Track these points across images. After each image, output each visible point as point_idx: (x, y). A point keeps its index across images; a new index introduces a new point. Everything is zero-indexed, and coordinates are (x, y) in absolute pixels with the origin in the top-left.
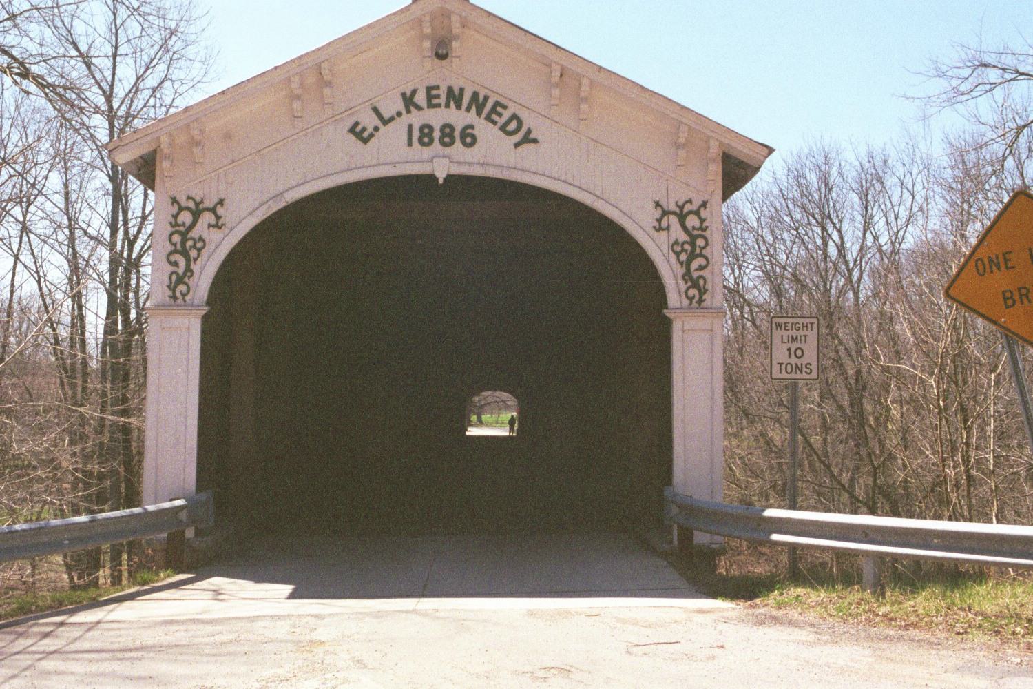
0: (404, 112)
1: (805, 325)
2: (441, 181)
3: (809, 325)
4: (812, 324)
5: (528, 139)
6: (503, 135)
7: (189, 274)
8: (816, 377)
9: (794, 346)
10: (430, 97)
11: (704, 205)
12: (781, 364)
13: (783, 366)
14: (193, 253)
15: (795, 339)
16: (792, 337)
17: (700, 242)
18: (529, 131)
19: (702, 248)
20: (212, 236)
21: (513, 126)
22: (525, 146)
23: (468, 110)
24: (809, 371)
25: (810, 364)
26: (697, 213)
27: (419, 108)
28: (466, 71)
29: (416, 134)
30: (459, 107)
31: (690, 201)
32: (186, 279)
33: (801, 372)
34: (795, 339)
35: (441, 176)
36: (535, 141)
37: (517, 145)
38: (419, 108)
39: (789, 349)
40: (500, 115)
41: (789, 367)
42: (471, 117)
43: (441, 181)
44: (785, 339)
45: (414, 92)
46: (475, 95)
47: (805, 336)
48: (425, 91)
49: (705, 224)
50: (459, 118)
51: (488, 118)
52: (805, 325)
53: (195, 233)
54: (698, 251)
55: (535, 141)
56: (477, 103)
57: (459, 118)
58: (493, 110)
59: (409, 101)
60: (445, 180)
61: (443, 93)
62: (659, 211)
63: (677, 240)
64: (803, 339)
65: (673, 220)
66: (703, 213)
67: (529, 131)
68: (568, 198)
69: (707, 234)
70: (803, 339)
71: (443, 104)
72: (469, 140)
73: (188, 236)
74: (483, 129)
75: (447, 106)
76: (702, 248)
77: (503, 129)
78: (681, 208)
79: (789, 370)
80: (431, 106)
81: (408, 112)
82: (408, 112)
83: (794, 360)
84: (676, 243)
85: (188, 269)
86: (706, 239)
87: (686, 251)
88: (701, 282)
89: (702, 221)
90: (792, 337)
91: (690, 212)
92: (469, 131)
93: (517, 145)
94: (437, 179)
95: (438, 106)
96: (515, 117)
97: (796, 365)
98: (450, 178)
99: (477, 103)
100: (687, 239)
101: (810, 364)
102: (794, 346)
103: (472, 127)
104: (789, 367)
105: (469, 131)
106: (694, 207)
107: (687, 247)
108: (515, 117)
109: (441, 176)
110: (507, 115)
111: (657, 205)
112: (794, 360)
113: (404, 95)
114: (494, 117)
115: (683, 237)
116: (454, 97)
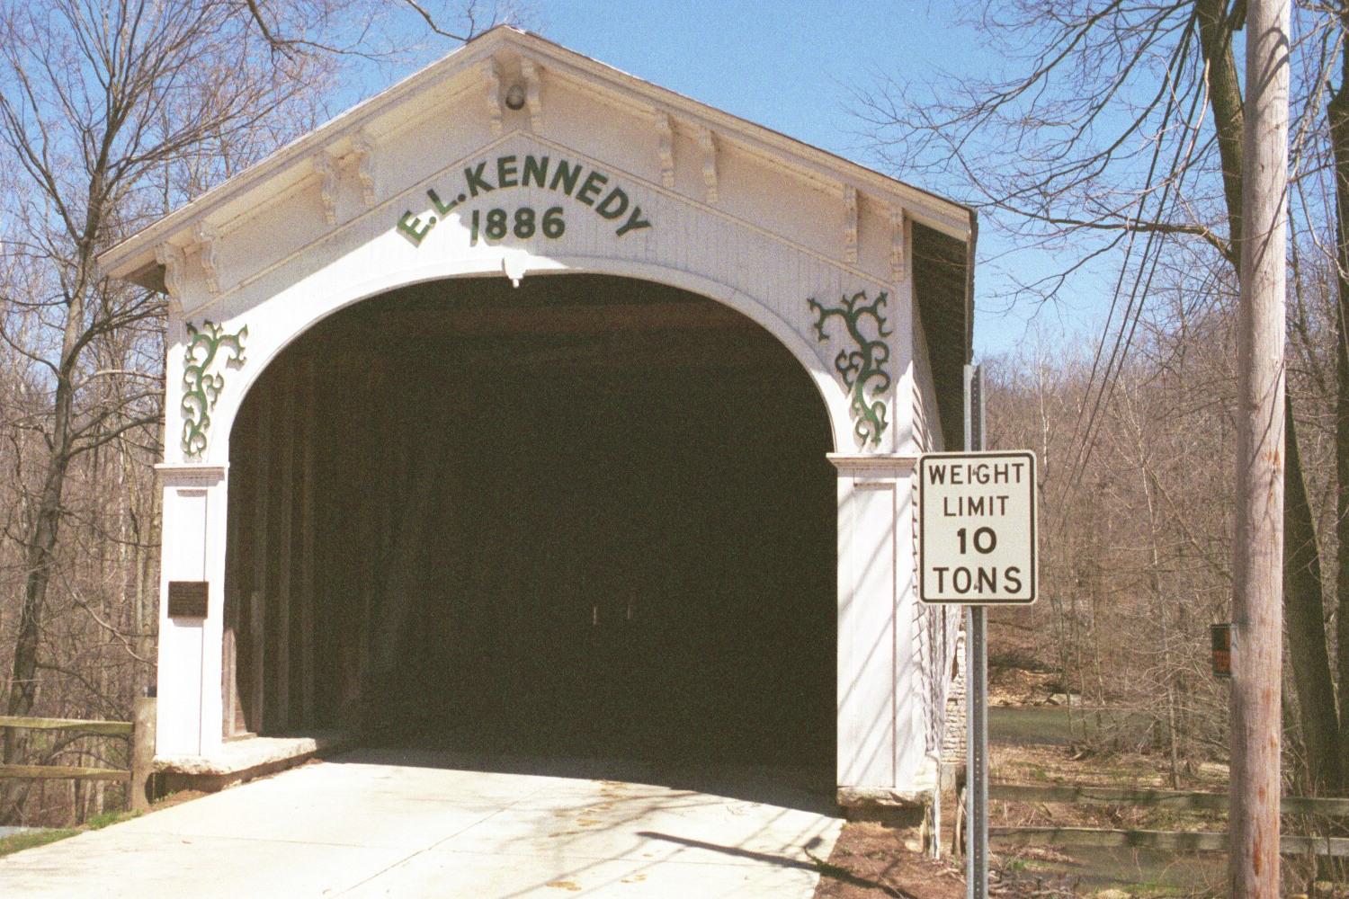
0: (467, 192)
1: (1001, 469)
2: (516, 284)
3: (1012, 471)
4: (1018, 466)
5: (635, 223)
6: (601, 218)
7: (205, 422)
8: (1028, 596)
9: (972, 523)
10: (503, 172)
11: (882, 298)
12: (941, 570)
13: (948, 576)
14: (210, 399)
15: (976, 507)
16: (970, 500)
17: (877, 353)
18: (637, 211)
19: (880, 362)
20: (230, 375)
21: (614, 205)
22: (631, 232)
23: (554, 186)
24: (1013, 586)
25: (1017, 571)
26: (872, 311)
27: (488, 188)
28: (547, 134)
29: (483, 223)
30: (541, 183)
31: (862, 294)
32: (202, 430)
33: (993, 587)
34: (976, 507)
35: (516, 276)
36: (646, 224)
37: (620, 232)
38: (488, 188)
39: (962, 533)
40: (597, 191)
41: (962, 577)
42: (558, 197)
43: (516, 284)
44: (953, 508)
45: (481, 167)
46: (563, 166)
47: (1003, 498)
48: (496, 164)
49: (887, 327)
50: (540, 199)
51: (582, 196)
52: (1001, 469)
53: (211, 371)
54: (874, 366)
55: (646, 224)
56: (566, 176)
57: (540, 199)
58: (588, 185)
59: (475, 180)
60: (521, 282)
61: (520, 165)
62: (817, 313)
63: (843, 351)
64: (997, 503)
65: (835, 325)
66: (882, 311)
67: (637, 211)
68: (750, 319)
69: (888, 341)
70: (997, 503)
71: (520, 181)
72: (554, 228)
73: (204, 375)
74: (577, 214)
75: (526, 183)
76: (880, 362)
77: (601, 210)
78: (851, 305)
79: (962, 585)
80: (503, 184)
81: (474, 193)
82: (474, 193)
83: (973, 560)
84: (842, 355)
85: (204, 417)
86: (886, 348)
87: (856, 367)
88: (878, 414)
89: (881, 321)
90: (970, 500)
91: (861, 310)
92: (554, 216)
93: (620, 232)
94: (510, 282)
95: (514, 183)
96: (618, 192)
97: (981, 572)
98: (528, 279)
99: (566, 176)
100: (856, 347)
101: (1017, 571)
102: (972, 523)
103: (559, 210)
104: (962, 577)
105: (554, 216)
106: (869, 303)
107: (857, 361)
108: (618, 192)
109: (516, 276)
110: (606, 190)
111: (813, 303)
112: (973, 560)
113: (468, 172)
114: (589, 194)
115: (852, 346)
116: (535, 169)
